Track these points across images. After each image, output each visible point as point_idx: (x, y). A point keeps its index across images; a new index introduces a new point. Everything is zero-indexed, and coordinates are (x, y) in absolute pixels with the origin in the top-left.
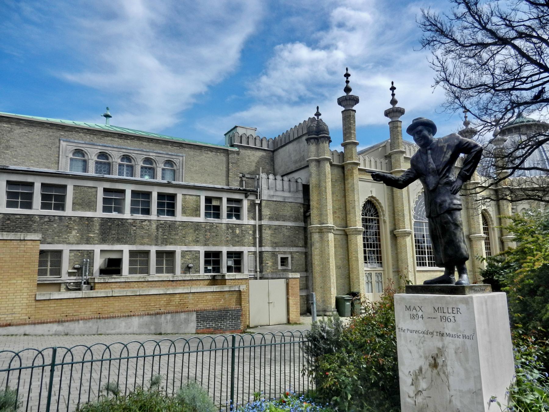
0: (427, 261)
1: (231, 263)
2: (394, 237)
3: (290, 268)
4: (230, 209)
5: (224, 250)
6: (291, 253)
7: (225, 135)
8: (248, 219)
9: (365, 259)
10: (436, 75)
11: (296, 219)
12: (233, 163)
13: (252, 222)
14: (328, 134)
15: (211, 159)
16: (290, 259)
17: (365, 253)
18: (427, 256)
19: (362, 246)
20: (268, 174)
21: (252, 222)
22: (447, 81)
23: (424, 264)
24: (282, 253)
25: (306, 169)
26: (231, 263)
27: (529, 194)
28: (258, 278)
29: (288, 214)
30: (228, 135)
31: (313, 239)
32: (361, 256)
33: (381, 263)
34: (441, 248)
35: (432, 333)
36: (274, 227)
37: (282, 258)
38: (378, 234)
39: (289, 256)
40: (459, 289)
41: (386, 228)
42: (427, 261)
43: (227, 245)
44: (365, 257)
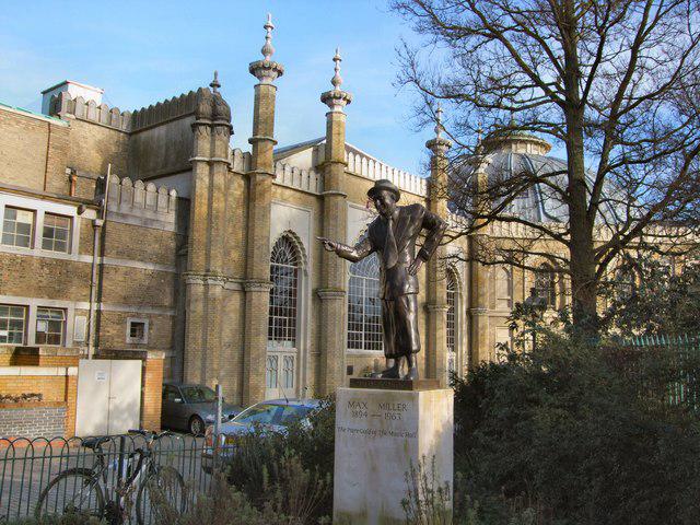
0: (363, 341)
1: (43, 327)
2: (319, 297)
3: (145, 341)
4: (48, 233)
5: (34, 303)
6: (149, 316)
7: (44, 93)
8: (80, 253)
9: (270, 334)
10: (396, 69)
11: (160, 260)
12: (57, 148)
13: (88, 259)
14: (229, 121)
15: (15, 136)
16: (146, 327)
17: (271, 323)
18: (363, 333)
19: (267, 313)
20: (121, 177)
21: (88, 259)
22: (417, 82)
23: (358, 346)
24: (133, 316)
25: (187, 175)
26: (43, 327)
27: (498, 283)
28: (90, 356)
29: (149, 250)
30: (49, 96)
31: (188, 294)
32: (264, 327)
33: (294, 340)
34: (393, 337)
35: (457, 381)
36: (125, 270)
37: (133, 324)
38: (293, 293)
39: (146, 322)
40: (407, 384)
41: (307, 283)
42: (363, 341)
43: (39, 296)
44: (270, 329)
